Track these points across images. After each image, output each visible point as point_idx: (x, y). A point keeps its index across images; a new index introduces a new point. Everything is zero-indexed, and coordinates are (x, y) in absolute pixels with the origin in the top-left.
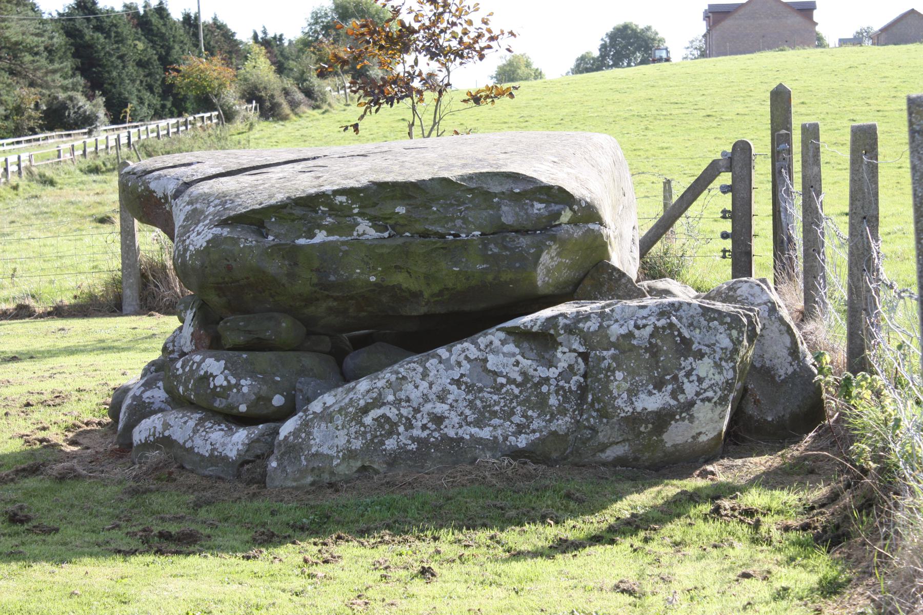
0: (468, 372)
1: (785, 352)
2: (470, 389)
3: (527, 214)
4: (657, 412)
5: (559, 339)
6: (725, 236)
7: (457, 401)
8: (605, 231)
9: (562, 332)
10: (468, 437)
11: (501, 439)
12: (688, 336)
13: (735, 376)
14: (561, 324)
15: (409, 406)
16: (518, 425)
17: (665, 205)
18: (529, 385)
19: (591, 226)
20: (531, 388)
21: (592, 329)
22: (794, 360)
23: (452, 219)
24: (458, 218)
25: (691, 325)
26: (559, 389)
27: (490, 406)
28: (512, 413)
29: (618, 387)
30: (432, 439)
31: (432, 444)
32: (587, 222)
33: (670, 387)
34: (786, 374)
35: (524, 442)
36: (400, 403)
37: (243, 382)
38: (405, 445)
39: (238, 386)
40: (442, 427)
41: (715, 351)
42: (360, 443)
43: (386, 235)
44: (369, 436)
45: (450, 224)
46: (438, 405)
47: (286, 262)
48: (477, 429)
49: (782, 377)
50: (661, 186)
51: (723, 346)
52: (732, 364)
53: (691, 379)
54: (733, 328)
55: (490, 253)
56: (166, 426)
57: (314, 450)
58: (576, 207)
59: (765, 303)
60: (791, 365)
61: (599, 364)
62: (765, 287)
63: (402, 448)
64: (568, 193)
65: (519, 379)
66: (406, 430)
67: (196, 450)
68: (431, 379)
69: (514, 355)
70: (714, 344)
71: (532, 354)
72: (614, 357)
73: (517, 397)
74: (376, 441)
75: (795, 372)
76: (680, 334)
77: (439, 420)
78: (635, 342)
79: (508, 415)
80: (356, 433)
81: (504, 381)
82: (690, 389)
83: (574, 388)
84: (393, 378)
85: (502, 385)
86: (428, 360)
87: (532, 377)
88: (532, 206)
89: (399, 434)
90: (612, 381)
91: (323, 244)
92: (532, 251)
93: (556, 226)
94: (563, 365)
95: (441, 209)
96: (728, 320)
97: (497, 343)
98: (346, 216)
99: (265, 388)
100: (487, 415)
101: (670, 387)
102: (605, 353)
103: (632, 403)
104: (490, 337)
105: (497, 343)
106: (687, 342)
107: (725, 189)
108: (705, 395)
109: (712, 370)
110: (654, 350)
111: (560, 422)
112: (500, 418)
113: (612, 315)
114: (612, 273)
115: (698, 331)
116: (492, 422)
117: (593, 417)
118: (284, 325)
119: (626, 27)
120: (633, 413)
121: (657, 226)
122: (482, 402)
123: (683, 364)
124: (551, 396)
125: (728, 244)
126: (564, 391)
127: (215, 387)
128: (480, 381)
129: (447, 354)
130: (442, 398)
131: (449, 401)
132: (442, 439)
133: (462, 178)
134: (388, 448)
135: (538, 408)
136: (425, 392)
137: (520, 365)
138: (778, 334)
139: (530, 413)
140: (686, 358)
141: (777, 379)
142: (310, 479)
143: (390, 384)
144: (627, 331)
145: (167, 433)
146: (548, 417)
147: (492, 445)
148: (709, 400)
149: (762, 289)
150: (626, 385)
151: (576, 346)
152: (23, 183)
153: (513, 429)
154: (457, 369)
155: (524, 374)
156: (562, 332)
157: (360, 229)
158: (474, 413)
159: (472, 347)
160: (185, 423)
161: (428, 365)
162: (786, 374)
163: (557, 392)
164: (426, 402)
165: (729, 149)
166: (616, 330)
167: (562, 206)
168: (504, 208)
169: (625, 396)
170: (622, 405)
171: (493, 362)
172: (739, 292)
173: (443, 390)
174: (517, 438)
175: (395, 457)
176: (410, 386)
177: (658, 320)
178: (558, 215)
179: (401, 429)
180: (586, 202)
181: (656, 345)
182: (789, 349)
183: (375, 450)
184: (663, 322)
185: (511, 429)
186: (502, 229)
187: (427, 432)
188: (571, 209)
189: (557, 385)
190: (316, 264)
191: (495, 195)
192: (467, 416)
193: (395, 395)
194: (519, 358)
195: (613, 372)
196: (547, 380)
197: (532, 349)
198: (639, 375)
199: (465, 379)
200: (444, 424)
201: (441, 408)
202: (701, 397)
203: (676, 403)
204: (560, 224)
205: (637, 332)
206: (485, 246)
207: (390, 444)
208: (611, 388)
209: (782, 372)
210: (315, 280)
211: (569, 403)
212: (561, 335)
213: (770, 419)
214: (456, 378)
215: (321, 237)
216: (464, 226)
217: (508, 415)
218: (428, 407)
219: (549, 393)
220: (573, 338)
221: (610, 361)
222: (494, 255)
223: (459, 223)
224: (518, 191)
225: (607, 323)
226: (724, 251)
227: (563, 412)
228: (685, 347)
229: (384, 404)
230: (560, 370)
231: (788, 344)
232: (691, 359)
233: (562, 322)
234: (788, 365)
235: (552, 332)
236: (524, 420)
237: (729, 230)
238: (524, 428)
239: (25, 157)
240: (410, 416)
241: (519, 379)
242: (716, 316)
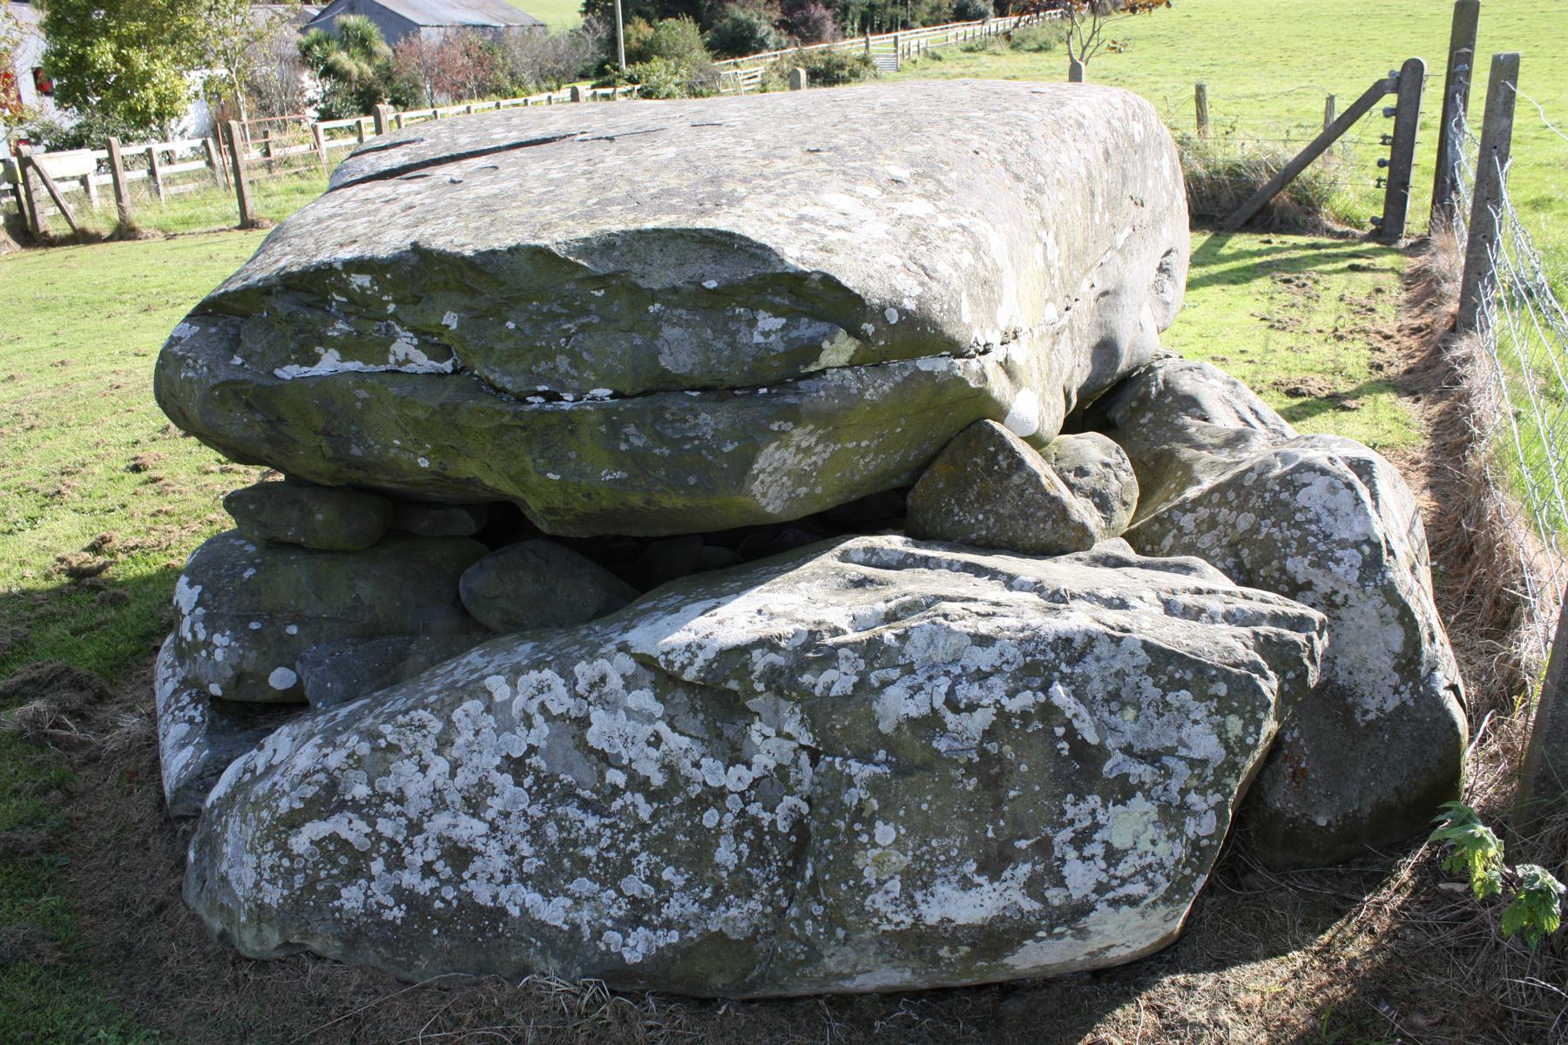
0: (543, 744)
1: (1387, 662)
2: (544, 788)
3: (733, 345)
4: (982, 927)
5: (753, 704)
6: (1382, 164)
7: (507, 815)
8: (968, 369)
9: (760, 687)
10: (515, 912)
11: (587, 932)
12: (1092, 737)
13: (1219, 830)
14: (759, 668)
15: (401, 814)
16: (634, 901)
17: (1326, 121)
18: (677, 800)
19: (925, 364)
20: (680, 808)
21: (836, 690)
22: (1404, 682)
23: (548, 355)
24: (562, 351)
25: (1114, 696)
26: (746, 822)
27: (575, 843)
28: (626, 868)
29: (879, 863)
30: (438, 904)
31: (437, 915)
32: (914, 355)
33: (1025, 869)
34: (1381, 710)
35: (641, 948)
36: (381, 805)
38: (381, 906)
40: (466, 875)
41: (1169, 774)
42: (278, 892)
43: (447, 366)
44: (299, 881)
45: (543, 367)
46: (464, 820)
47: (259, 417)
48: (538, 897)
49: (1370, 717)
51: (1197, 754)
52: (1219, 797)
53: (1087, 852)
54: (1233, 711)
55: (623, 447)
58: (869, 328)
59: (1357, 545)
60: (1396, 691)
61: (837, 792)
62: (1364, 493)
63: (373, 912)
64: (847, 290)
65: (658, 780)
66: (389, 870)
68: (455, 753)
69: (650, 719)
70: (1171, 752)
71: (695, 723)
72: (874, 786)
73: (644, 827)
74: (320, 888)
75: (1402, 709)
76: (1071, 733)
77: (459, 855)
78: (941, 745)
79: (613, 874)
80: (272, 869)
81: (616, 777)
82: (1080, 877)
83: (783, 827)
84: (364, 748)
85: (616, 791)
86: (461, 701)
87: (688, 780)
88: (752, 323)
89: (371, 878)
90: (863, 846)
91: (335, 377)
92: (729, 448)
93: (810, 375)
94: (763, 761)
95: (527, 329)
96: (1222, 689)
97: (615, 682)
98: (375, 319)
99: (252, 655)
100: (567, 863)
101: (1025, 869)
102: (855, 767)
103: (914, 906)
104: (602, 664)
105: (615, 682)
106: (1087, 757)
107: (1388, 113)
108: (1121, 892)
109: (1152, 832)
110: (991, 772)
111: (733, 912)
112: (594, 878)
113: (900, 651)
114: (995, 455)
115: (1130, 713)
116: (573, 887)
117: (814, 919)
118: (319, 517)
120: (914, 925)
121: (1308, 149)
122: (561, 828)
123: (1071, 812)
124: (722, 842)
125: (1384, 173)
126: (759, 831)
128: (569, 769)
129: (507, 690)
130: (474, 807)
131: (490, 814)
132: (461, 906)
133: (586, 248)
134: (347, 906)
135: (691, 865)
136: (439, 784)
137: (663, 747)
138: (1375, 622)
139: (668, 874)
140: (1080, 798)
141: (1358, 716)
143: (356, 761)
144: (925, 710)
146: (707, 895)
147: (564, 944)
148: (1132, 901)
149: (1358, 501)
150: (900, 860)
151: (791, 727)
152: (920, 59)
153: (620, 910)
154: (521, 731)
155: (669, 768)
156: (760, 687)
158: (537, 855)
159: (558, 683)
161: (457, 714)
162: (1381, 710)
163: (738, 833)
164: (437, 809)
165: (1398, 69)
166: (897, 704)
167: (824, 327)
168: (669, 332)
169: (895, 886)
170: (887, 909)
171: (602, 728)
172: (1302, 498)
173: (481, 785)
174: (626, 936)
175: (358, 930)
176: (409, 767)
177: (1012, 694)
178: (812, 350)
179: (377, 866)
180: (903, 312)
181: (1000, 758)
182: (1397, 656)
183: (318, 908)
184: (1026, 699)
185: (614, 912)
186: (665, 385)
187: (431, 883)
188: (854, 332)
189: (742, 813)
190: (320, 422)
191: (653, 296)
192: (523, 858)
193: (371, 783)
194: (662, 727)
195: (870, 823)
196: (718, 795)
197: (694, 711)
198: (940, 833)
199: (534, 760)
200: (472, 868)
201: (469, 829)
202: (1110, 895)
203: (1037, 906)
204: (823, 371)
205: (950, 718)
206: (615, 429)
207: (351, 897)
208: (859, 863)
209: (1372, 704)
210: (329, 452)
211: (762, 865)
212: (755, 694)
213: (1322, 822)
214: (516, 754)
215: (329, 362)
216: (573, 372)
217: (613, 874)
218: (441, 821)
219: (719, 833)
220: (786, 707)
221: (863, 795)
222: (633, 453)
223: (563, 362)
224: (711, 284)
225: (882, 674)
226: (1379, 180)
227: (745, 889)
228: (1082, 768)
229: (342, 806)
230: (756, 772)
231: (1397, 646)
232: (1094, 800)
233: (760, 660)
234: (1387, 691)
235: (733, 685)
236: (650, 890)
237: (1388, 158)
238: (647, 910)
239: (923, 41)
240: (400, 839)
241: (658, 780)
242: (1189, 676)
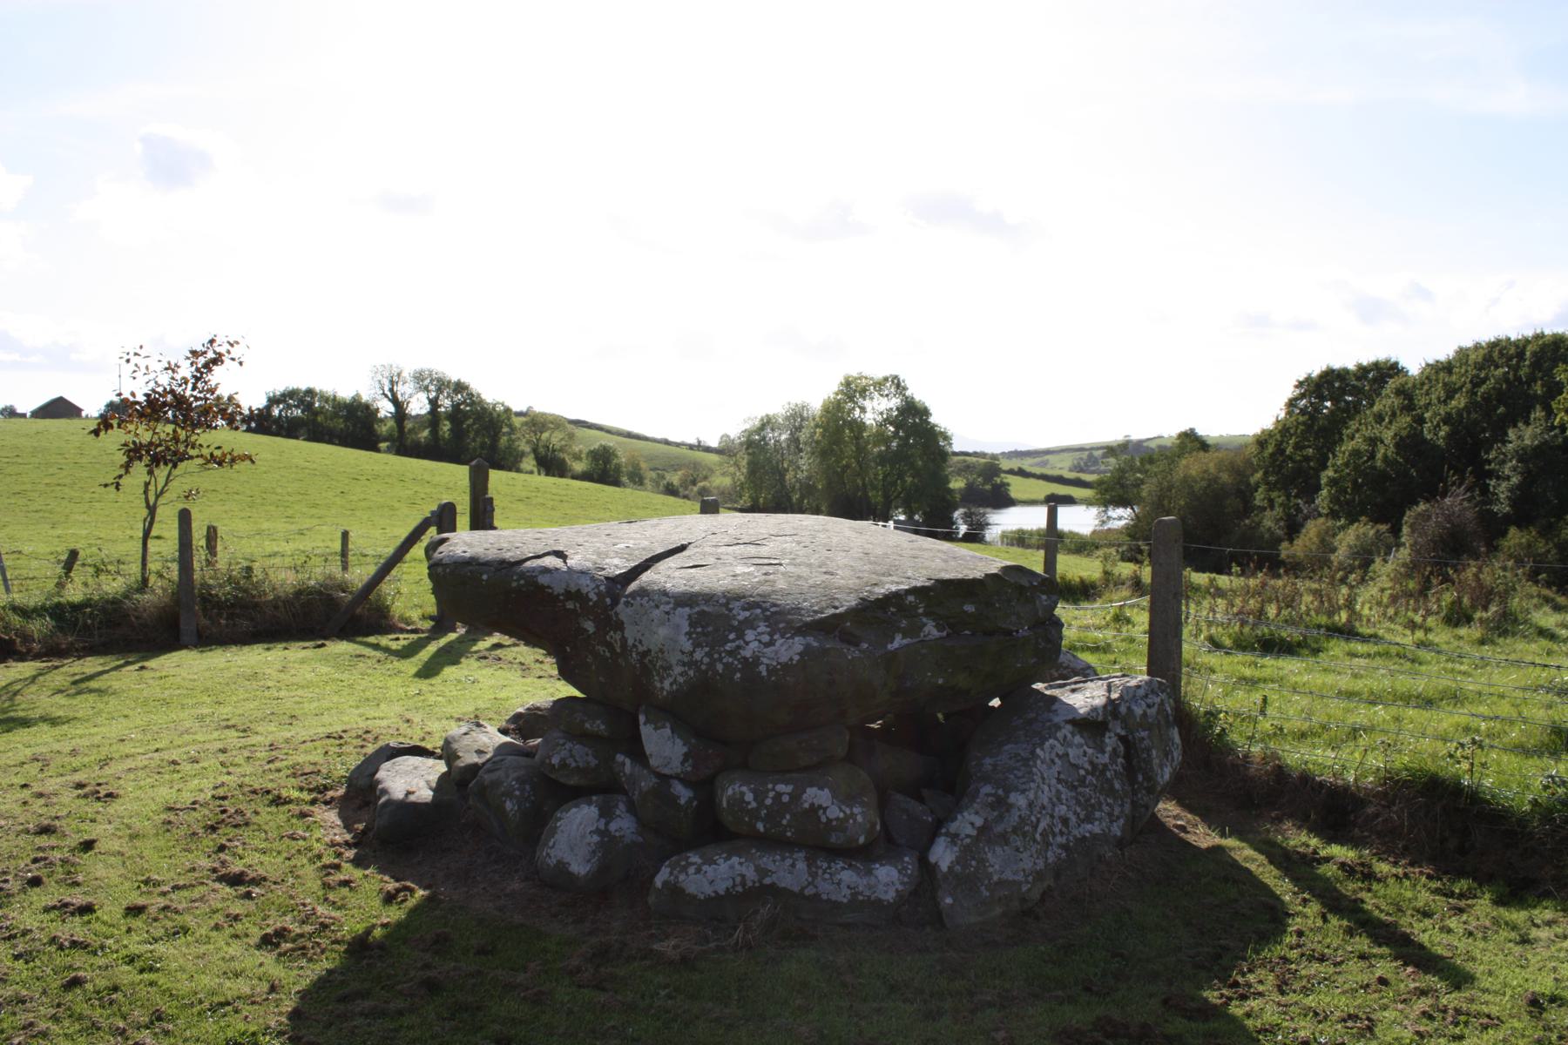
37: (855, 810)
39: (853, 815)
50: (339, 535)
56: (762, 872)
57: (995, 878)
67: (824, 897)
119: (1192, 430)
127: (829, 821)
142: (998, 910)
145: (767, 881)
157: (926, 629)
160: (793, 865)
